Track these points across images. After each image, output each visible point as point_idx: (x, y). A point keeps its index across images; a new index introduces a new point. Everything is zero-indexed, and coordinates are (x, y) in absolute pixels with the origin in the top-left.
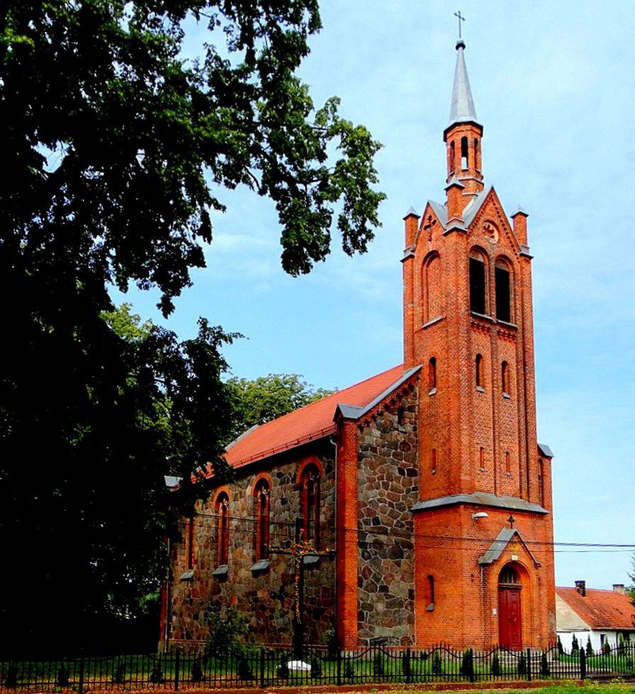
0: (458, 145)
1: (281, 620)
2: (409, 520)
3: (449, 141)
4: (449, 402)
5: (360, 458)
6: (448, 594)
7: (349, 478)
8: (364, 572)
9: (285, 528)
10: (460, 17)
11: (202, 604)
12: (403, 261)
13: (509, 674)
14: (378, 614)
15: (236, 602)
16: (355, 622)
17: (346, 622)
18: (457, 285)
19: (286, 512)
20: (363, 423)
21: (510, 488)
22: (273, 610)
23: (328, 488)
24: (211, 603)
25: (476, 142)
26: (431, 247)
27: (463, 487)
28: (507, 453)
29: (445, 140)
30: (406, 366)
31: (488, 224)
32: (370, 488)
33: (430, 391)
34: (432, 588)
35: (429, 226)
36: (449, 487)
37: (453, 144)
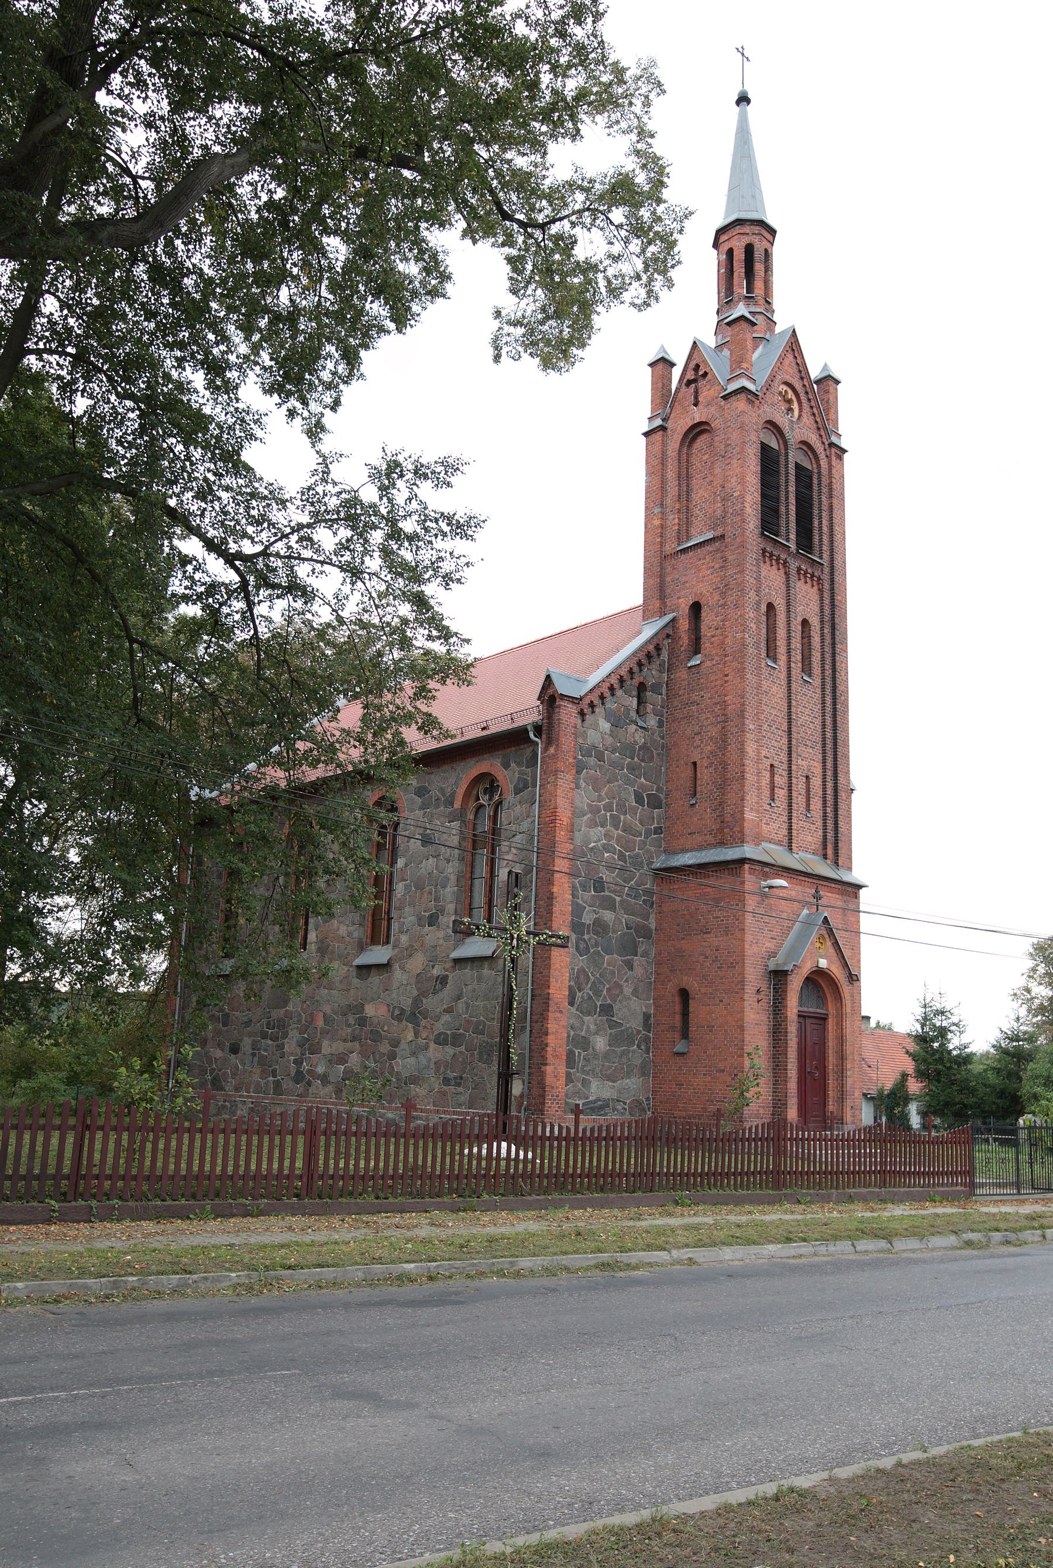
0: (739, 256)
1: (412, 1060)
2: (648, 886)
3: (725, 247)
4: (726, 682)
5: (580, 767)
6: (550, 1031)
7: (563, 806)
8: (578, 977)
9: (427, 889)
10: (743, 54)
11: (248, 1023)
12: (646, 434)
13: (946, 1173)
14: (595, 1056)
15: (320, 1023)
16: (562, 1069)
17: (549, 1069)
18: (742, 481)
19: (431, 859)
20: (585, 706)
21: (809, 839)
22: (395, 1043)
23: (518, 820)
24: (268, 1024)
25: (767, 255)
26: (697, 415)
27: (747, 831)
28: (807, 777)
29: (716, 245)
30: (647, 611)
31: (785, 388)
32: (593, 824)
33: (689, 659)
34: (685, 1014)
35: (694, 381)
36: (721, 830)
37: (730, 253)
